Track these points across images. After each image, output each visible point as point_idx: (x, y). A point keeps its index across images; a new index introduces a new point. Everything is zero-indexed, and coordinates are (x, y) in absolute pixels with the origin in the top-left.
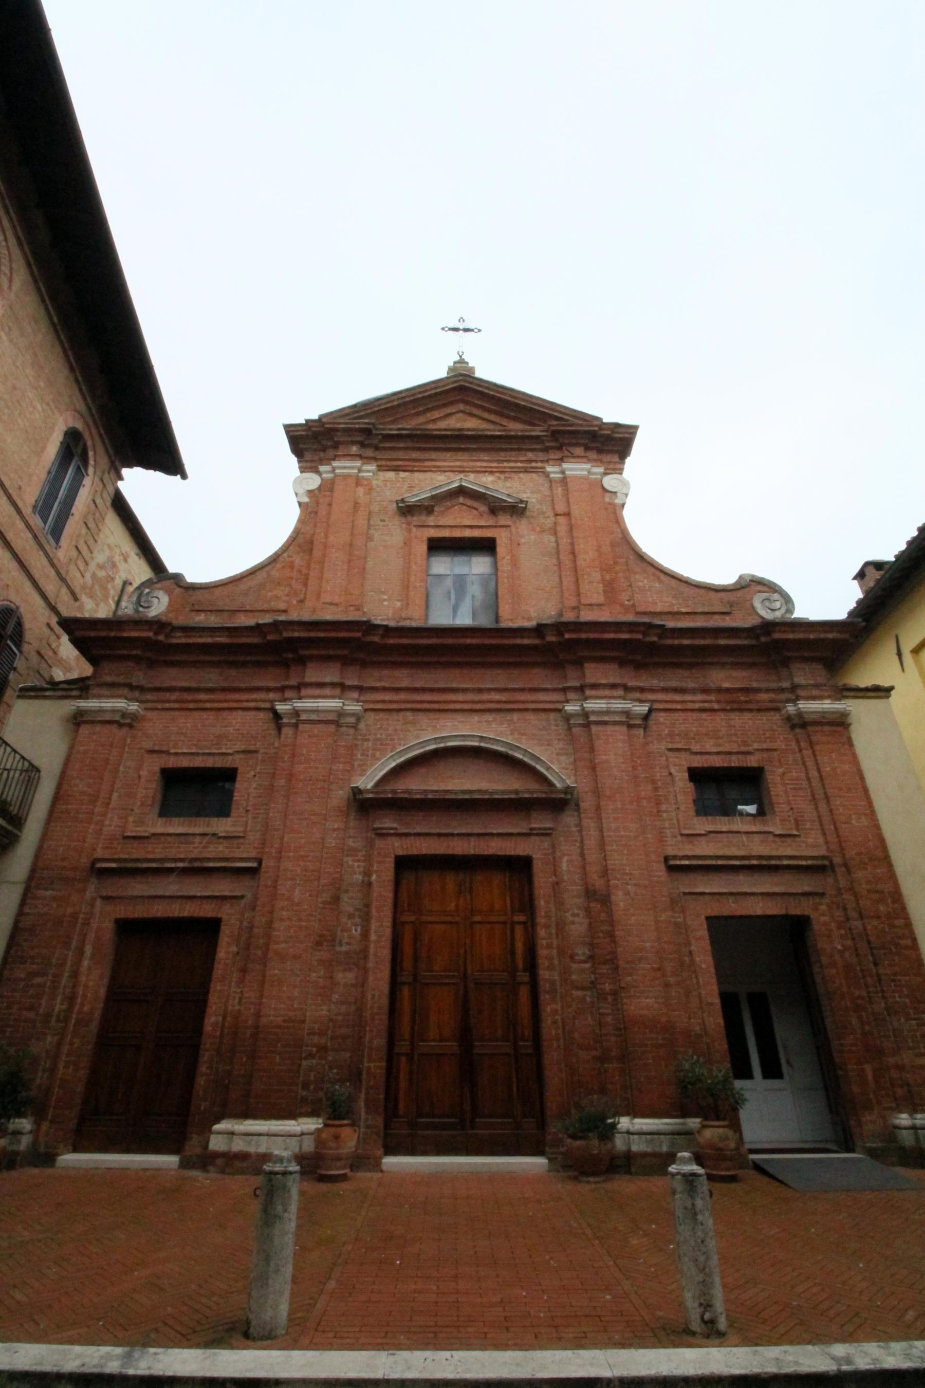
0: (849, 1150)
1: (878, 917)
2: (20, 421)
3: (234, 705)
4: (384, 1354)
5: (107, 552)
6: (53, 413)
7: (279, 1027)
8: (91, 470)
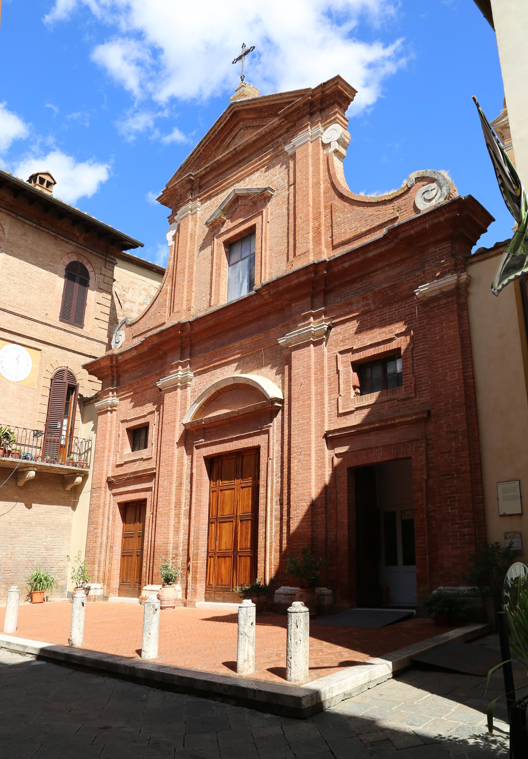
2: (34, 286)
5: (152, 288)
6: (53, 266)
7: (161, 546)
8: (91, 274)
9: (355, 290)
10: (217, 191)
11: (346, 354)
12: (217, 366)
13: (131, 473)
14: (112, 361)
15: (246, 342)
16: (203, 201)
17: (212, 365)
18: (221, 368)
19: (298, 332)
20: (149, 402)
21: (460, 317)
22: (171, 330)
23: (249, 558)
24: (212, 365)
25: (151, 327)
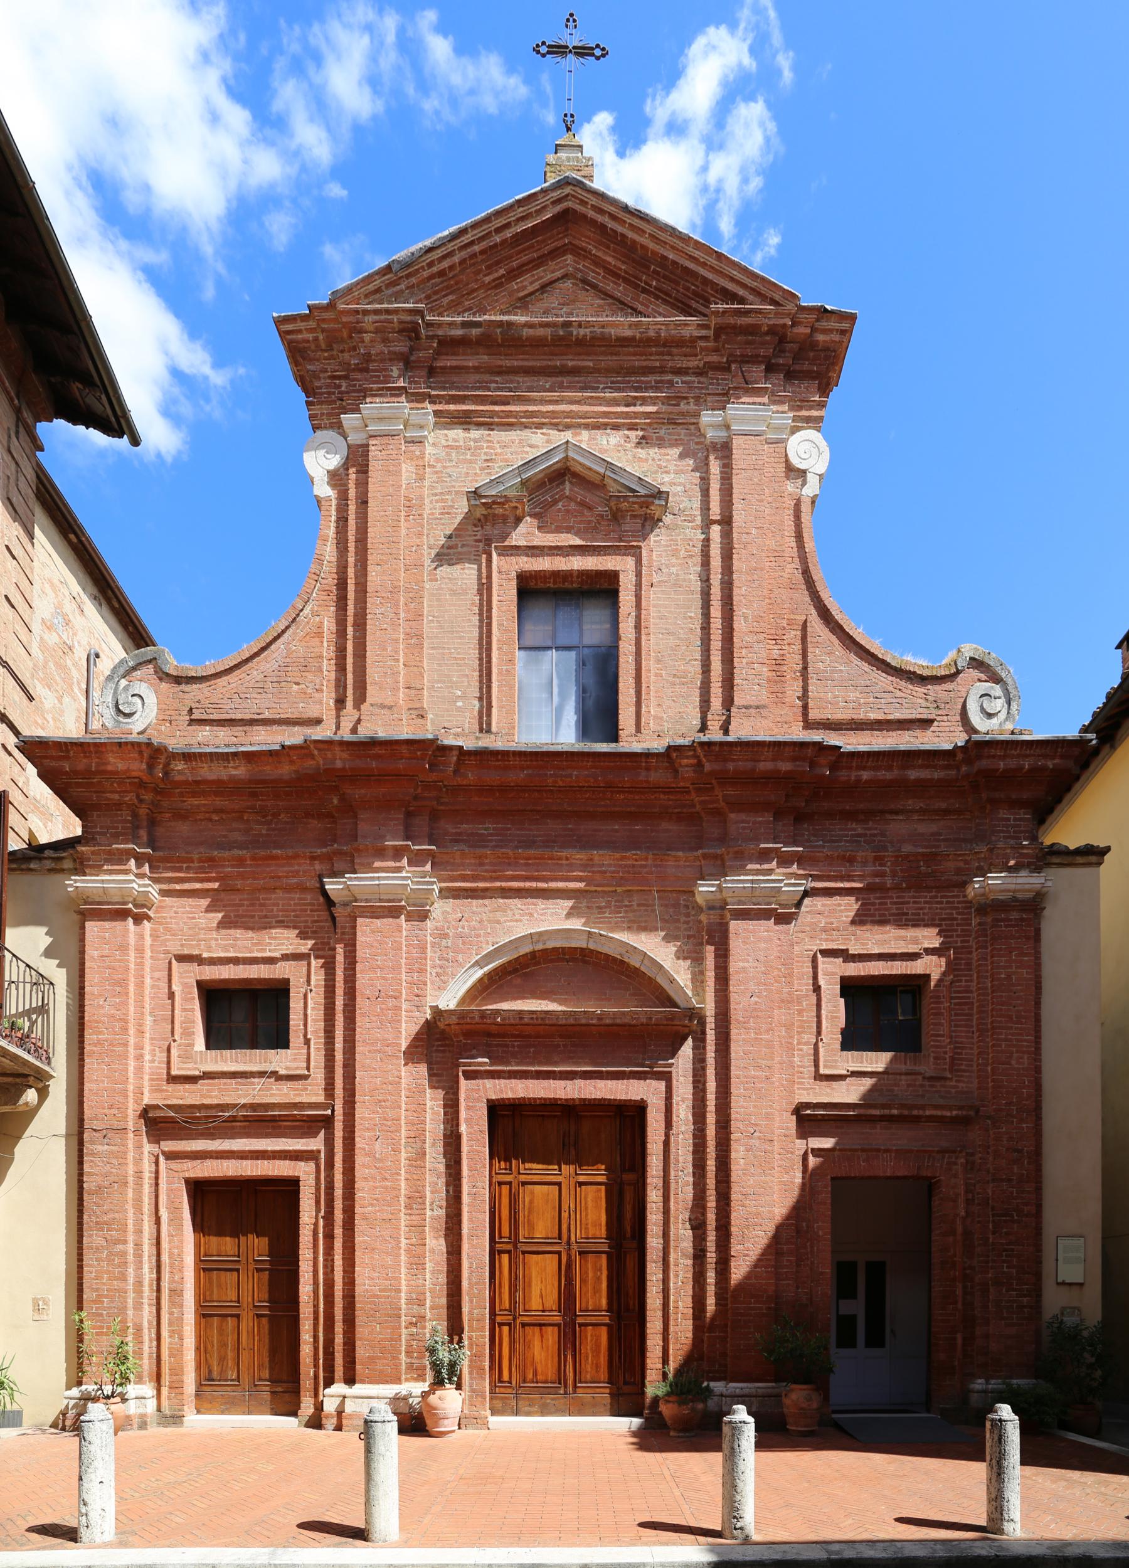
0: (928, 1411)
1: (1010, 1180)
4: (476, 1550)
7: (377, 1296)
9: (852, 836)
10: (493, 414)
11: (832, 959)
12: (511, 889)
13: (244, 1106)
14: (151, 766)
15: (604, 858)
16: (447, 420)
17: (498, 884)
18: (525, 900)
19: (752, 881)
20: (282, 924)
22: (404, 749)
23: (604, 1330)
24: (498, 884)
25: (267, 715)
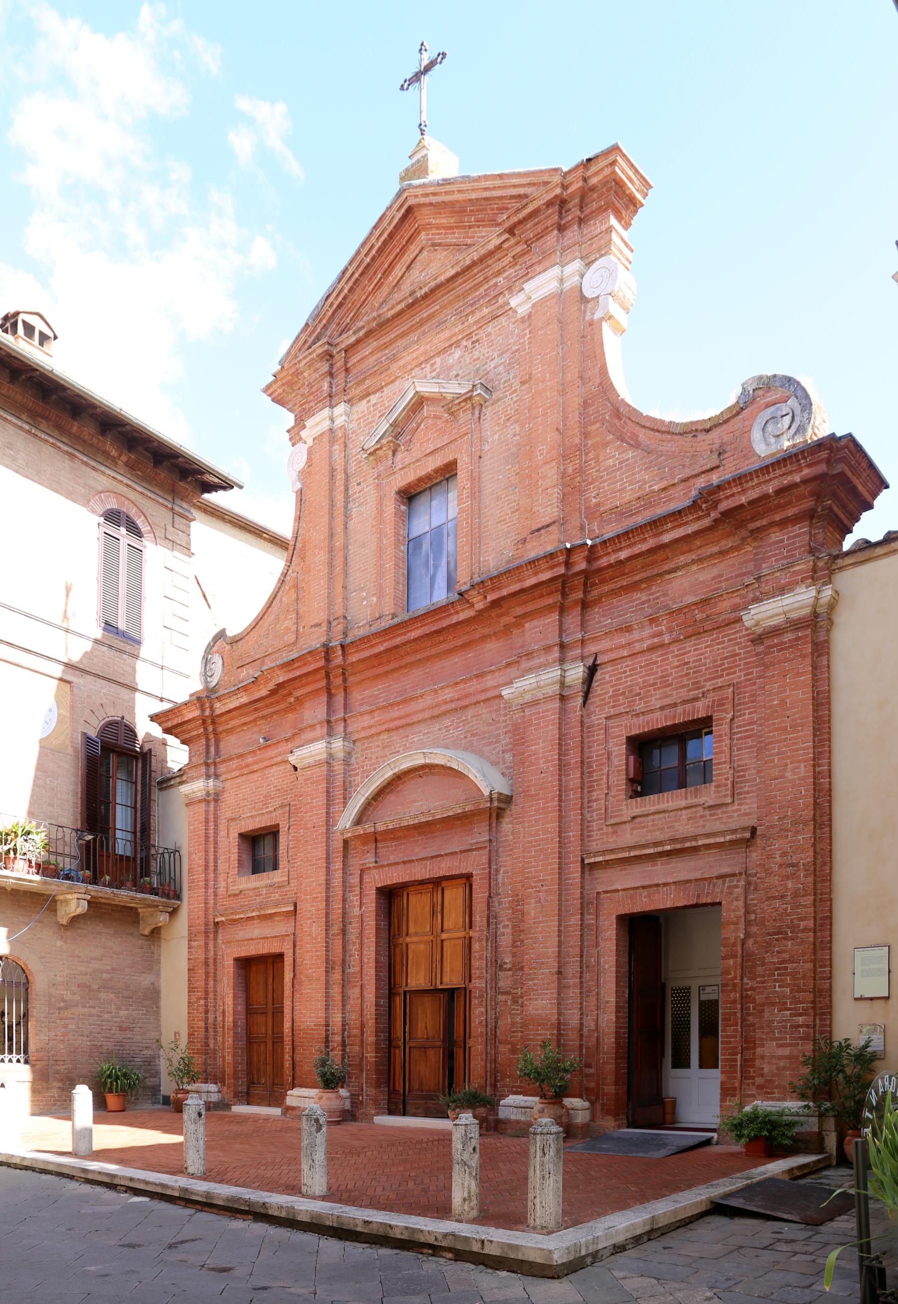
3: (268, 763)
7: (313, 1030)
21: (815, 667)
